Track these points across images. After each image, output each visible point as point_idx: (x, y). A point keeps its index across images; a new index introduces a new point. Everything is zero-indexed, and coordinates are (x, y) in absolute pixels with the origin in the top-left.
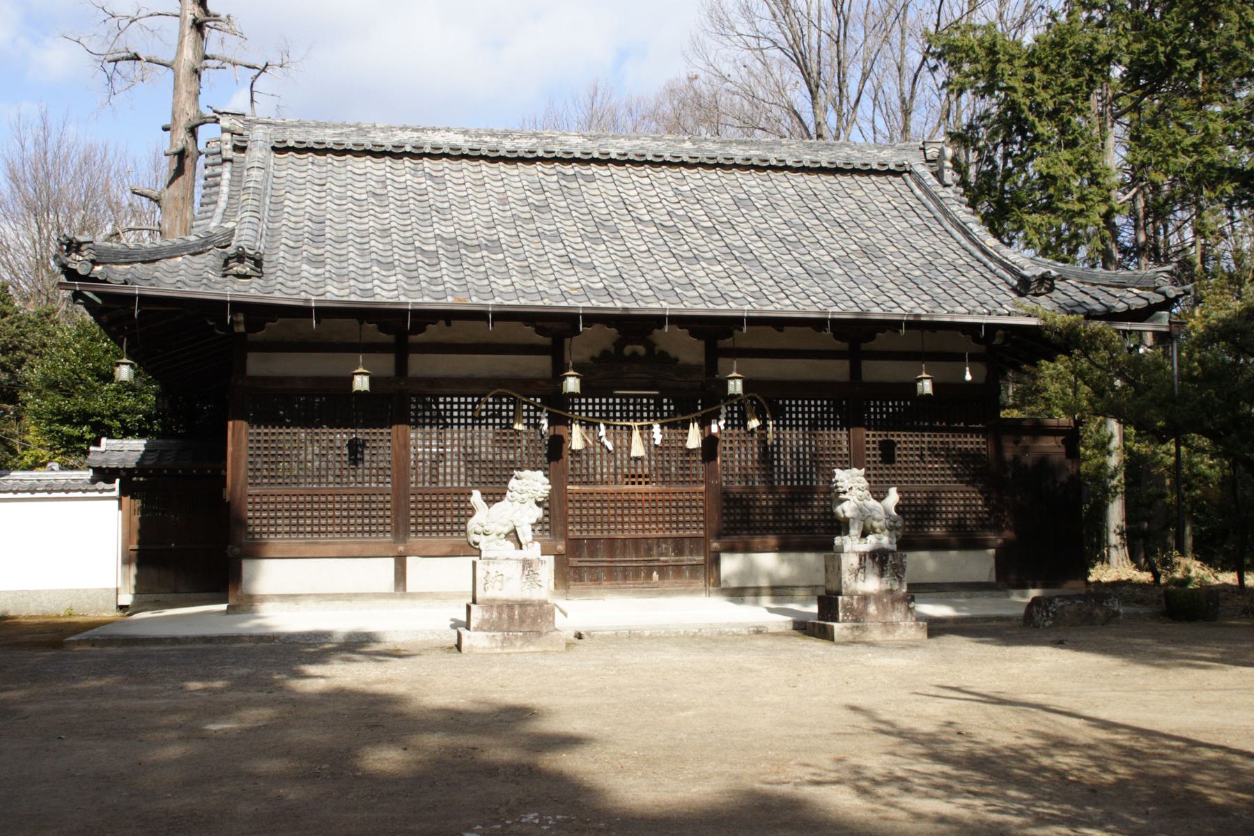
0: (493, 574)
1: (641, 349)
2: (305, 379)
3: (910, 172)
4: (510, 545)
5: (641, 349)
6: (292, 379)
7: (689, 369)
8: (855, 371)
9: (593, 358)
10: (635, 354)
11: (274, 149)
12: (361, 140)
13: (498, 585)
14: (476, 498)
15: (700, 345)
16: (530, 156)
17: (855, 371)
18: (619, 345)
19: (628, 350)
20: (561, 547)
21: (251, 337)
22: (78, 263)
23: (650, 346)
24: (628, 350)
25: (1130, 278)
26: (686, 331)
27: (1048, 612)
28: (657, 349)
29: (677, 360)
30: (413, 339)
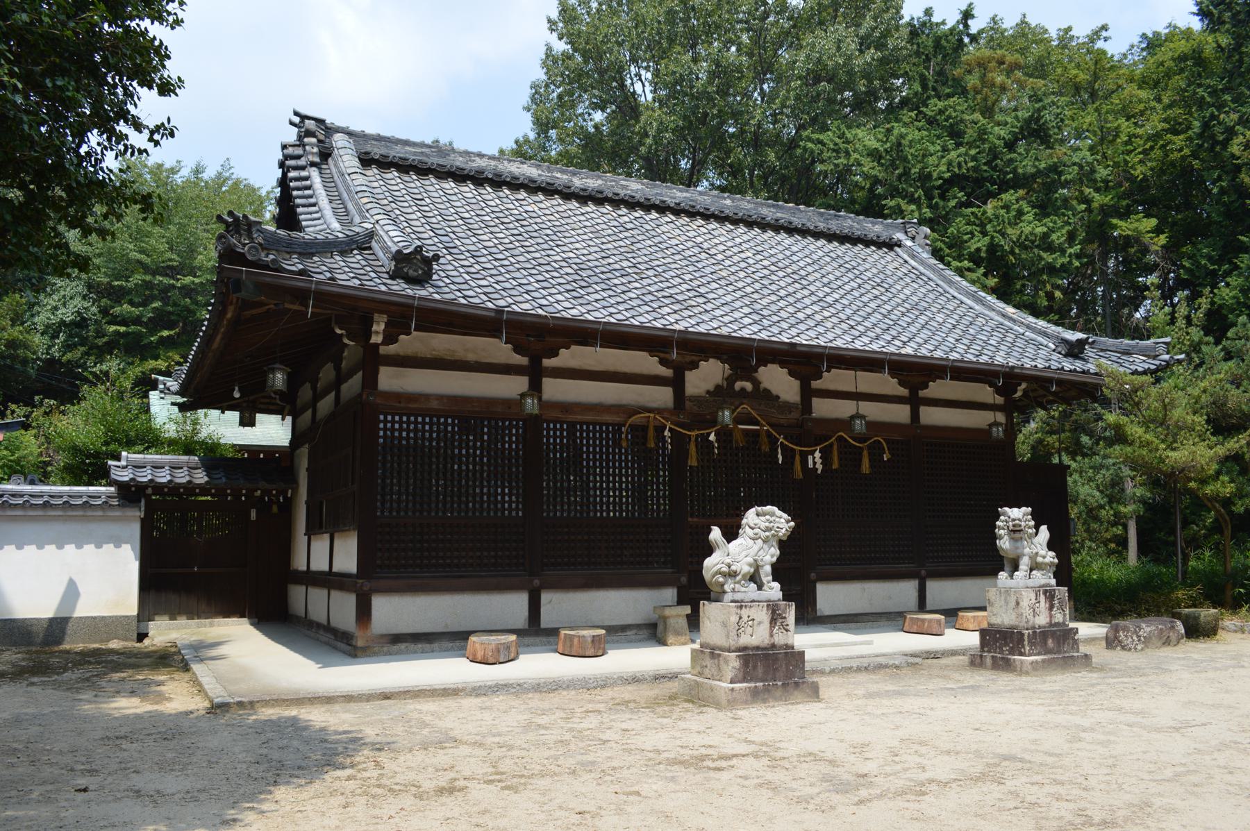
0: (745, 619)
1: (748, 386)
2: (440, 398)
3: (899, 246)
4: (753, 586)
5: (748, 386)
6: (427, 397)
7: (788, 406)
8: (915, 415)
9: (708, 392)
10: (743, 389)
11: (1104, 28)
12: (442, 161)
13: (749, 630)
14: (716, 534)
15: (796, 384)
16: (600, 196)
17: (915, 415)
18: (731, 380)
19: (738, 385)
20: (684, 580)
21: (383, 350)
22: (242, 245)
23: (756, 383)
24: (738, 385)
25: (1133, 347)
26: (785, 370)
27: (1139, 636)
28: (762, 386)
29: (778, 397)
30: (547, 362)
